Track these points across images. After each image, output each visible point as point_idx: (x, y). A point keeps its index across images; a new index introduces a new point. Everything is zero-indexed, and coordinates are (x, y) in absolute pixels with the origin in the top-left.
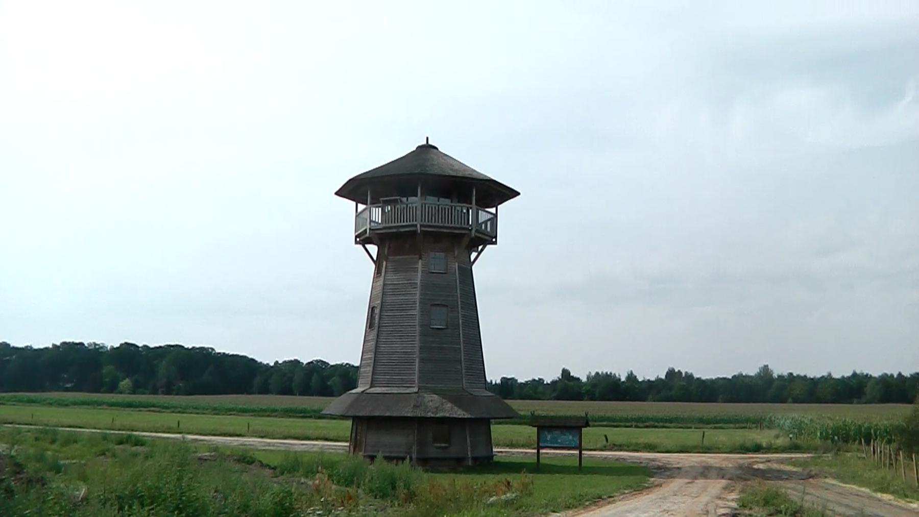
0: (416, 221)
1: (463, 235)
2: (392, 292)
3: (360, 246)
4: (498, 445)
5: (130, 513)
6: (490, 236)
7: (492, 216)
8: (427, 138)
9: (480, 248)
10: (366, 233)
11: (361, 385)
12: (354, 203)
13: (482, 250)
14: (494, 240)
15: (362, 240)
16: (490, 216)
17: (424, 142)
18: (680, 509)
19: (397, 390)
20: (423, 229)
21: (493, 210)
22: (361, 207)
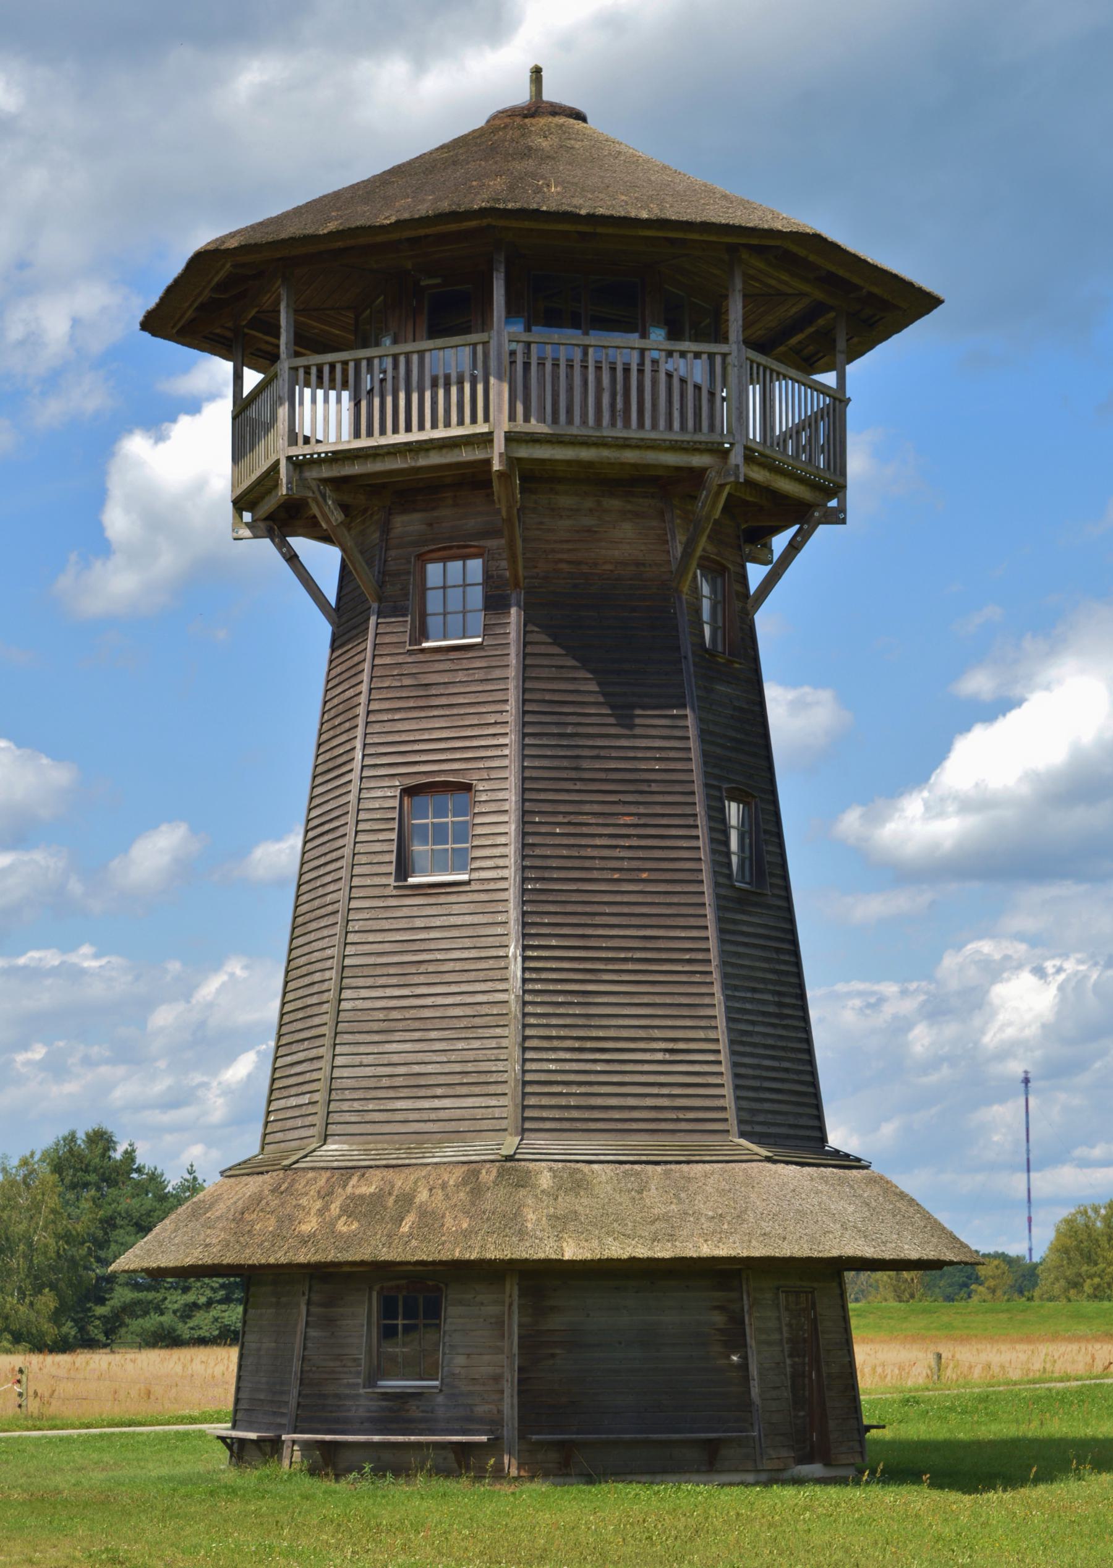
0: (486, 419)
1: (697, 476)
2: (755, 1077)
3: (266, 545)
4: (865, 1393)
5: (35, 1454)
6: (815, 486)
7: (823, 401)
8: (537, 72)
9: (780, 542)
10: (276, 485)
11: (863, 1322)
12: (228, 366)
13: (794, 548)
14: (833, 503)
15: (270, 518)
16: (823, 401)
17: (522, 96)
18: (977, 1350)
19: (377, 1105)
20: (523, 452)
21: (829, 379)
22: (252, 378)
